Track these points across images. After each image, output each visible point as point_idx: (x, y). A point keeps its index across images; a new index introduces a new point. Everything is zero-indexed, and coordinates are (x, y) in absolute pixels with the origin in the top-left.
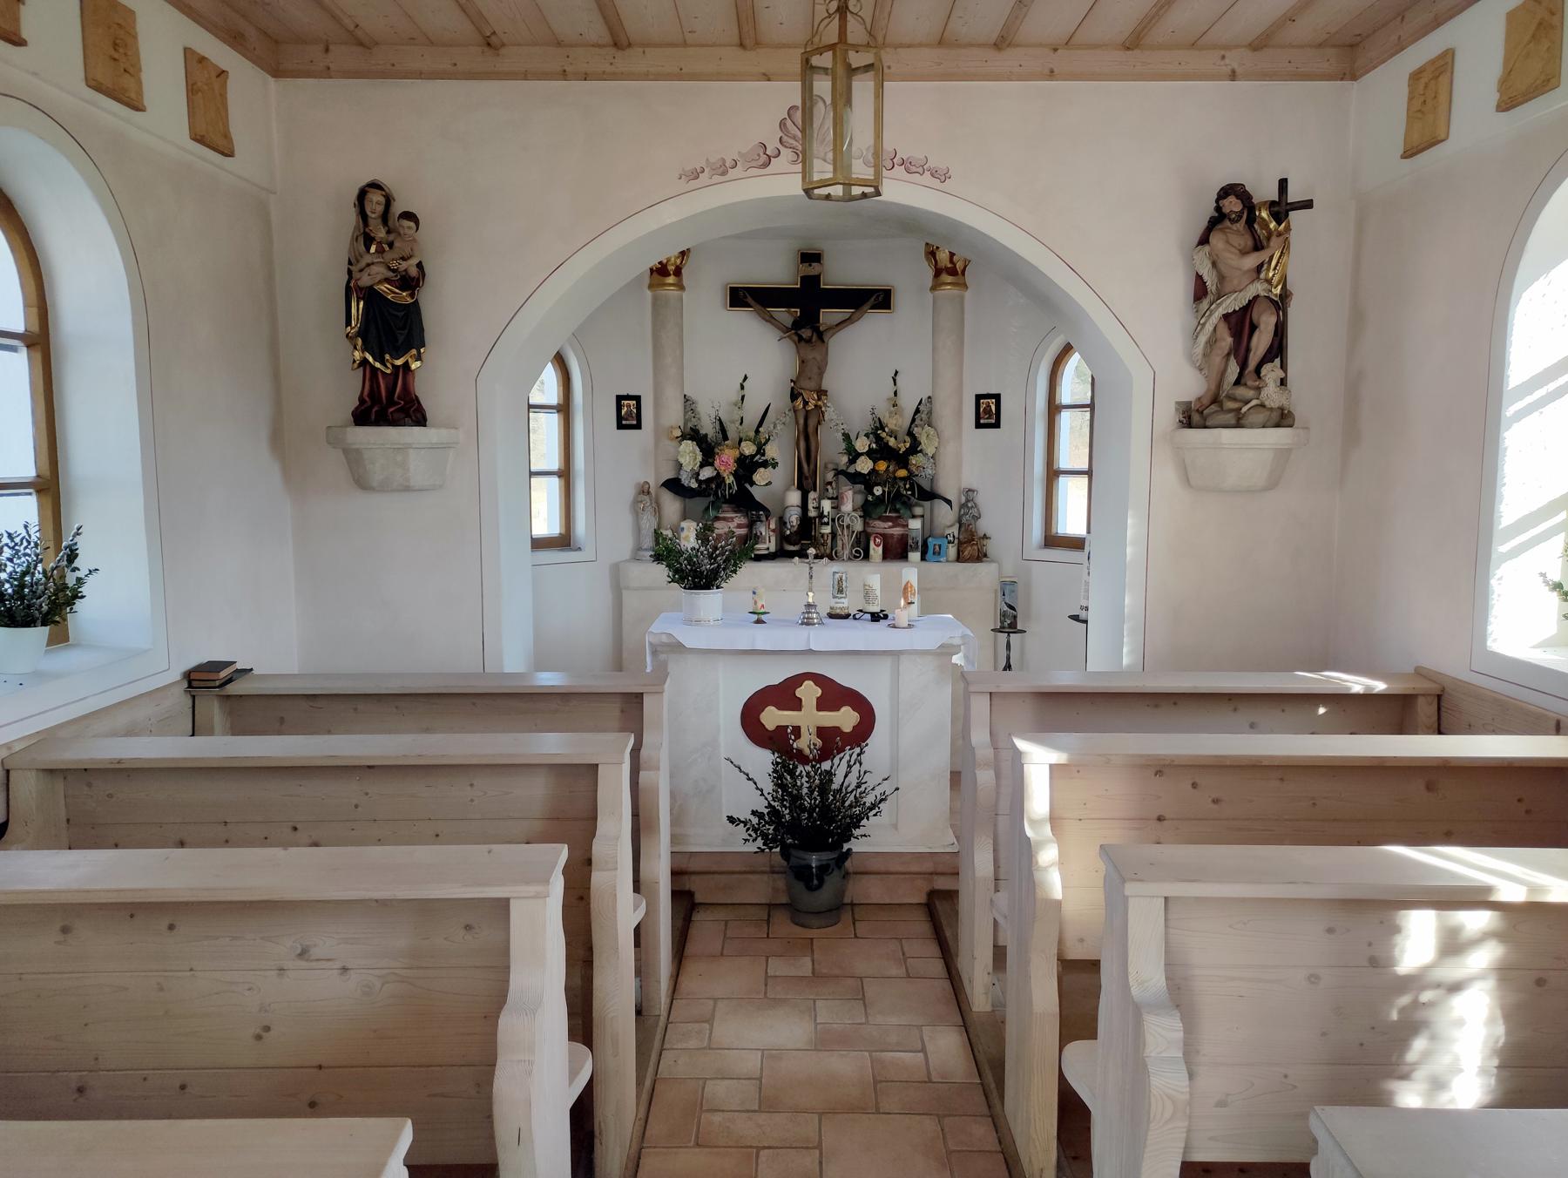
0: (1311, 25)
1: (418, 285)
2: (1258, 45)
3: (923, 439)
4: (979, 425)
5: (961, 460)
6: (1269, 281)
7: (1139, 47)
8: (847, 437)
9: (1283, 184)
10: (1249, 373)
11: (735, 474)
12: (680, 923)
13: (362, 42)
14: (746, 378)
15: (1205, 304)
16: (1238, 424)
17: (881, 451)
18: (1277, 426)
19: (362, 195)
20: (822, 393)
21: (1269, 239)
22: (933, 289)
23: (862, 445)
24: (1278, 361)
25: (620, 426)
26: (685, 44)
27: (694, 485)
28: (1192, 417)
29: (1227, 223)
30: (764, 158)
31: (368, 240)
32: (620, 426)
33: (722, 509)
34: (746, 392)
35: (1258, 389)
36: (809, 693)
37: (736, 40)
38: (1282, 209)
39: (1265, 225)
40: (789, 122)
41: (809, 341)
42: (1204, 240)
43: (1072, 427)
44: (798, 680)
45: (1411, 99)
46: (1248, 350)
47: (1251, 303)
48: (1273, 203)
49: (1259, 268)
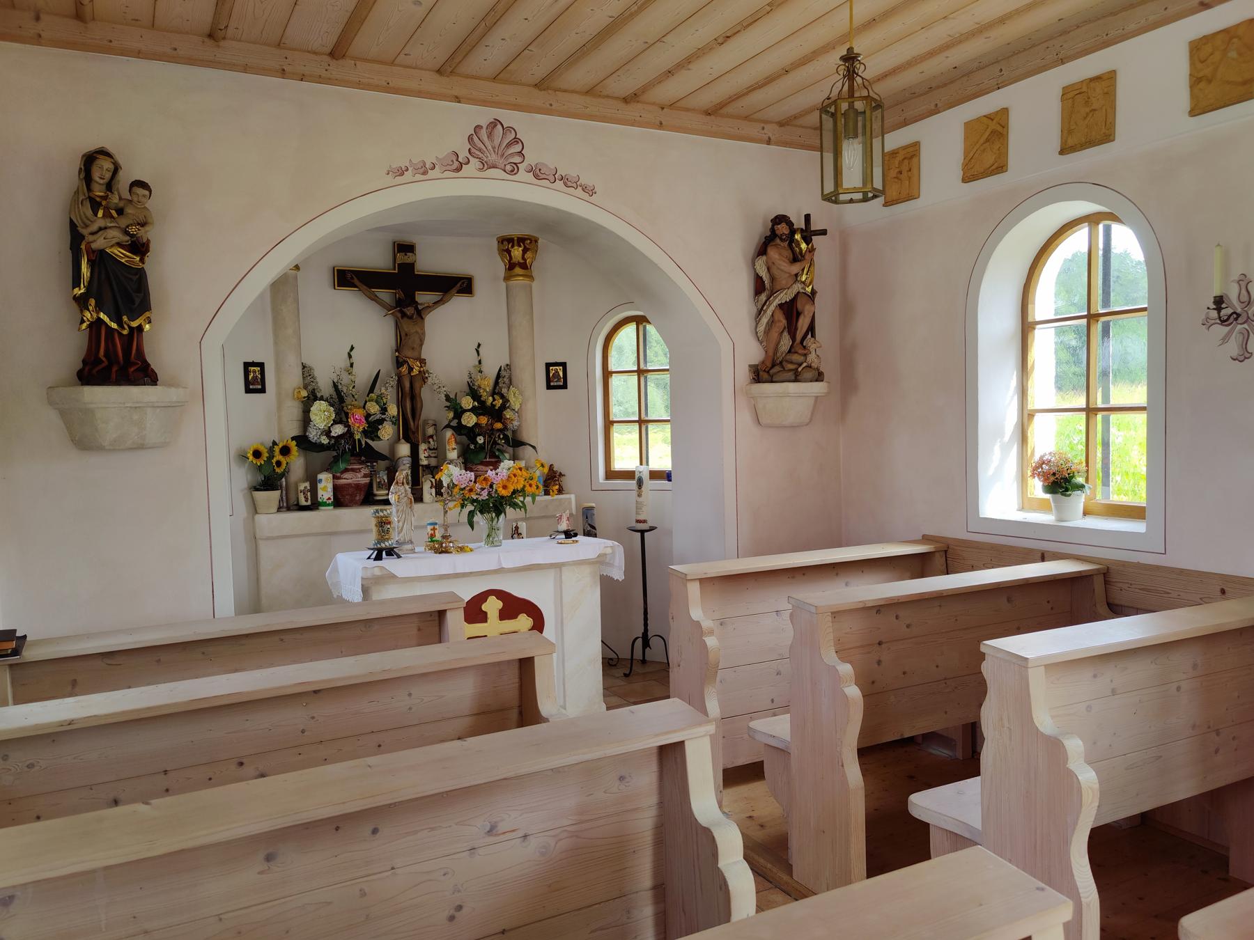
4: (549, 387)
9: (807, 217)
14: (352, 348)
15: (763, 297)
16: (796, 380)
19: (90, 160)
20: (423, 362)
25: (248, 391)
27: (325, 440)
28: (760, 374)
29: (778, 241)
30: (456, 164)
32: (248, 391)
34: (354, 359)
35: (805, 355)
36: (492, 606)
39: (798, 245)
40: (475, 138)
41: (411, 318)
44: (483, 597)
46: (796, 329)
47: (794, 300)
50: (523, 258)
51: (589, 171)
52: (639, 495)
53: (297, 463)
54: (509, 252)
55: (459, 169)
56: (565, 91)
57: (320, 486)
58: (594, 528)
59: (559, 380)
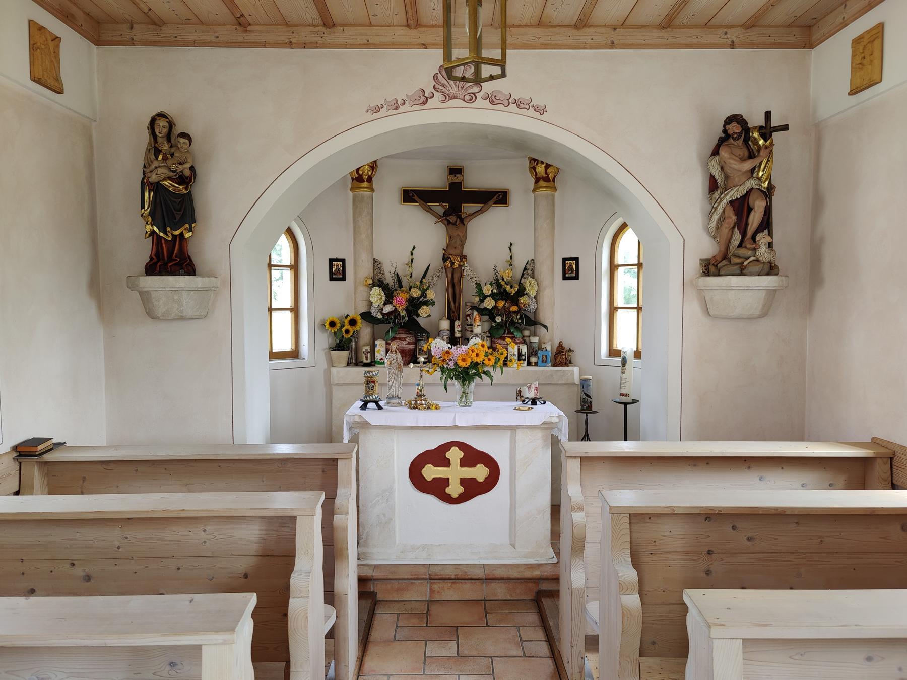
0: (779, 14)
1: (190, 181)
2: (751, 24)
3: (527, 286)
4: (565, 278)
5: (554, 302)
6: (760, 179)
7: (674, 28)
8: (478, 285)
9: (768, 115)
10: (748, 239)
11: (407, 310)
12: (365, 617)
13: (156, 22)
14: (414, 248)
15: (716, 195)
16: (742, 273)
17: (501, 294)
18: (768, 274)
20: (463, 257)
21: (759, 151)
22: (534, 191)
23: (487, 290)
24: (766, 232)
25: (332, 279)
26: (371, 25)
27: (380, 317)
28: (710, 268)
29: (731, 140)
30: (423, 99)
31: (157, 151)
32: (332, 279)
33: (389, 326)
35: (755, 250)
36: (455, 455)
37: (405, 22)
38: (768, 131)
39: (756, 142)
41: (454, 224)
42: (715, 152)
43: (626, 281)
44: (447, 447)
45: (854, 56)
46: (747, 224)
48: (761, 127)
49: (752, 171)
50: (546, 173)
51: (554, 97)
52: (623, 372)
53: (365, 331)
54: (534, 168)
55: (424, 103)
56: (519, 26)
57: (377, 349)
58: (589, 397)
59: (572, 273)
